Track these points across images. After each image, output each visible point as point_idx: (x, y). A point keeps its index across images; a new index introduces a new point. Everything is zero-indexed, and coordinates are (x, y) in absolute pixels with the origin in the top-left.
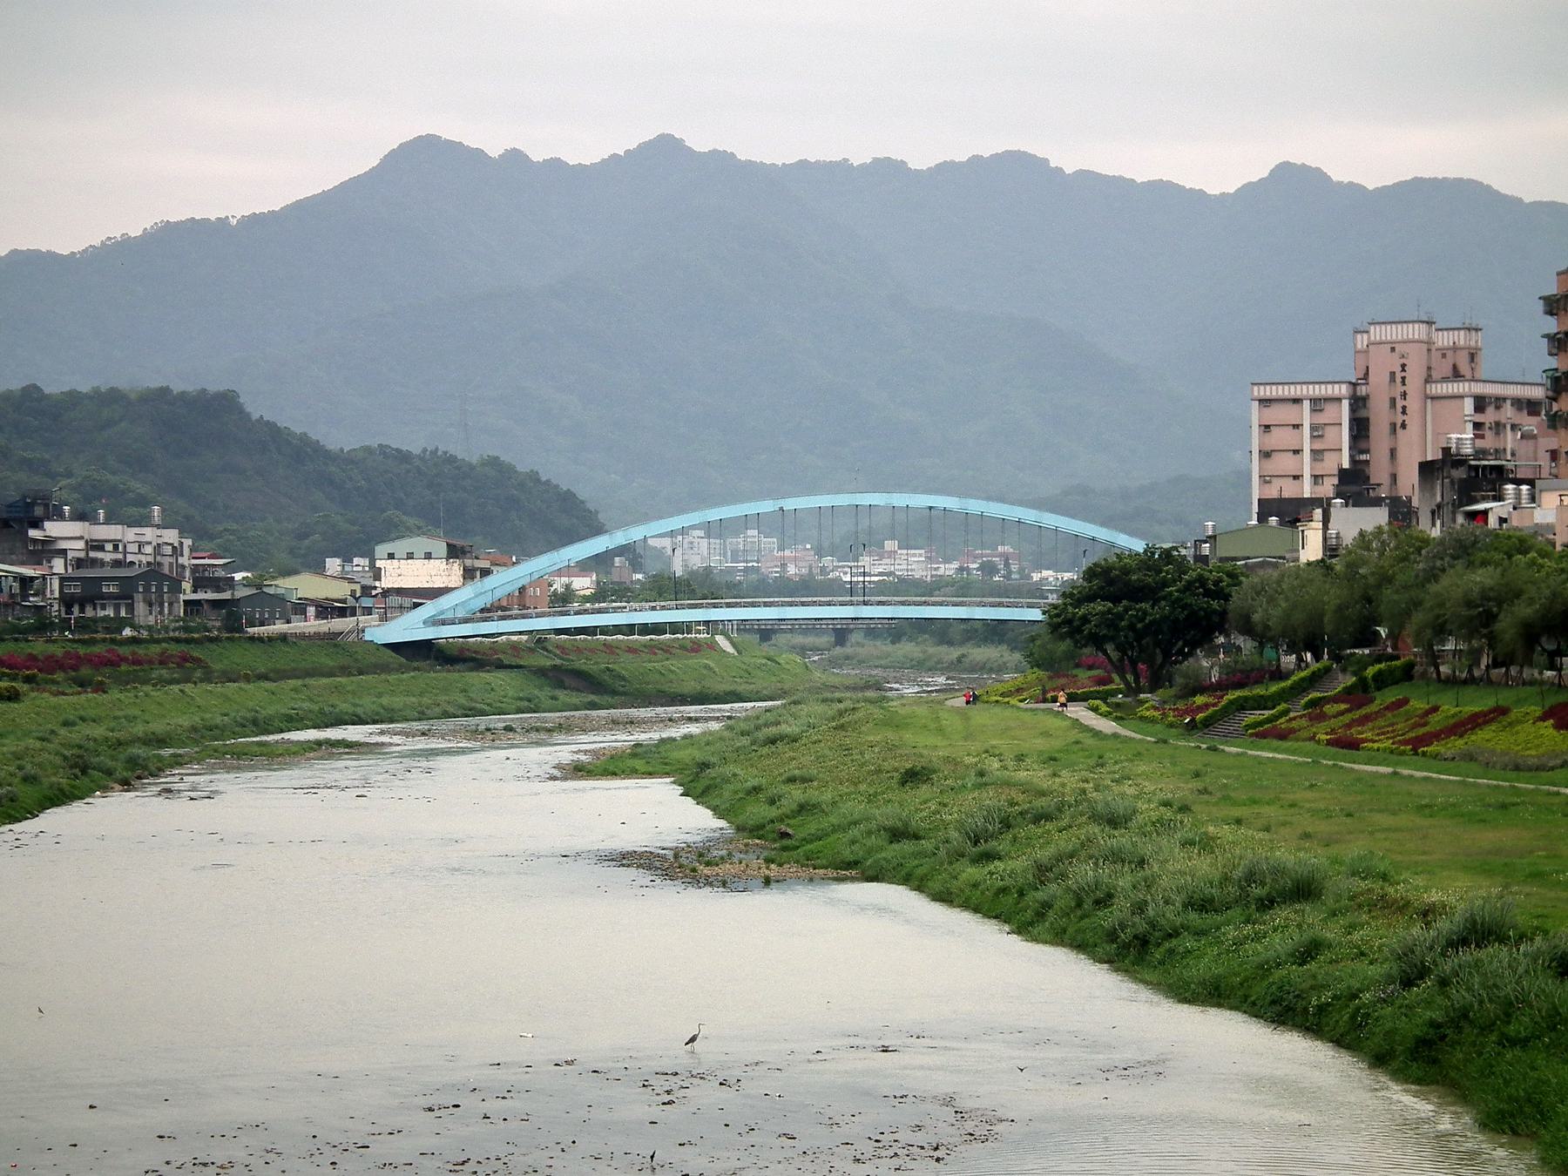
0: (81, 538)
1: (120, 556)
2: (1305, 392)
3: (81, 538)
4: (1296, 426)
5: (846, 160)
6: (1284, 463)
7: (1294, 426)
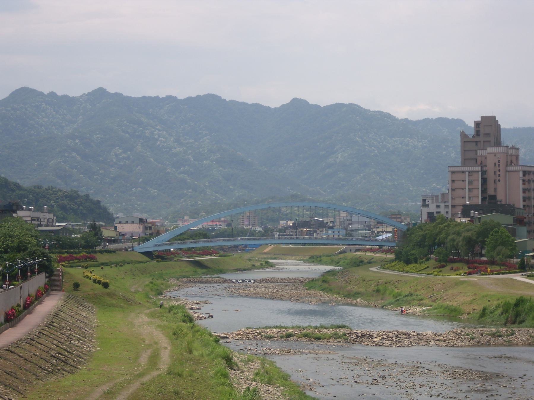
0: (30, 216)
1: (39, 223)
2: (466, 169)
3: (30, 216)
4: (463, 181)
5: (158, 96)
6: (459, 193)
7: (462, 180)
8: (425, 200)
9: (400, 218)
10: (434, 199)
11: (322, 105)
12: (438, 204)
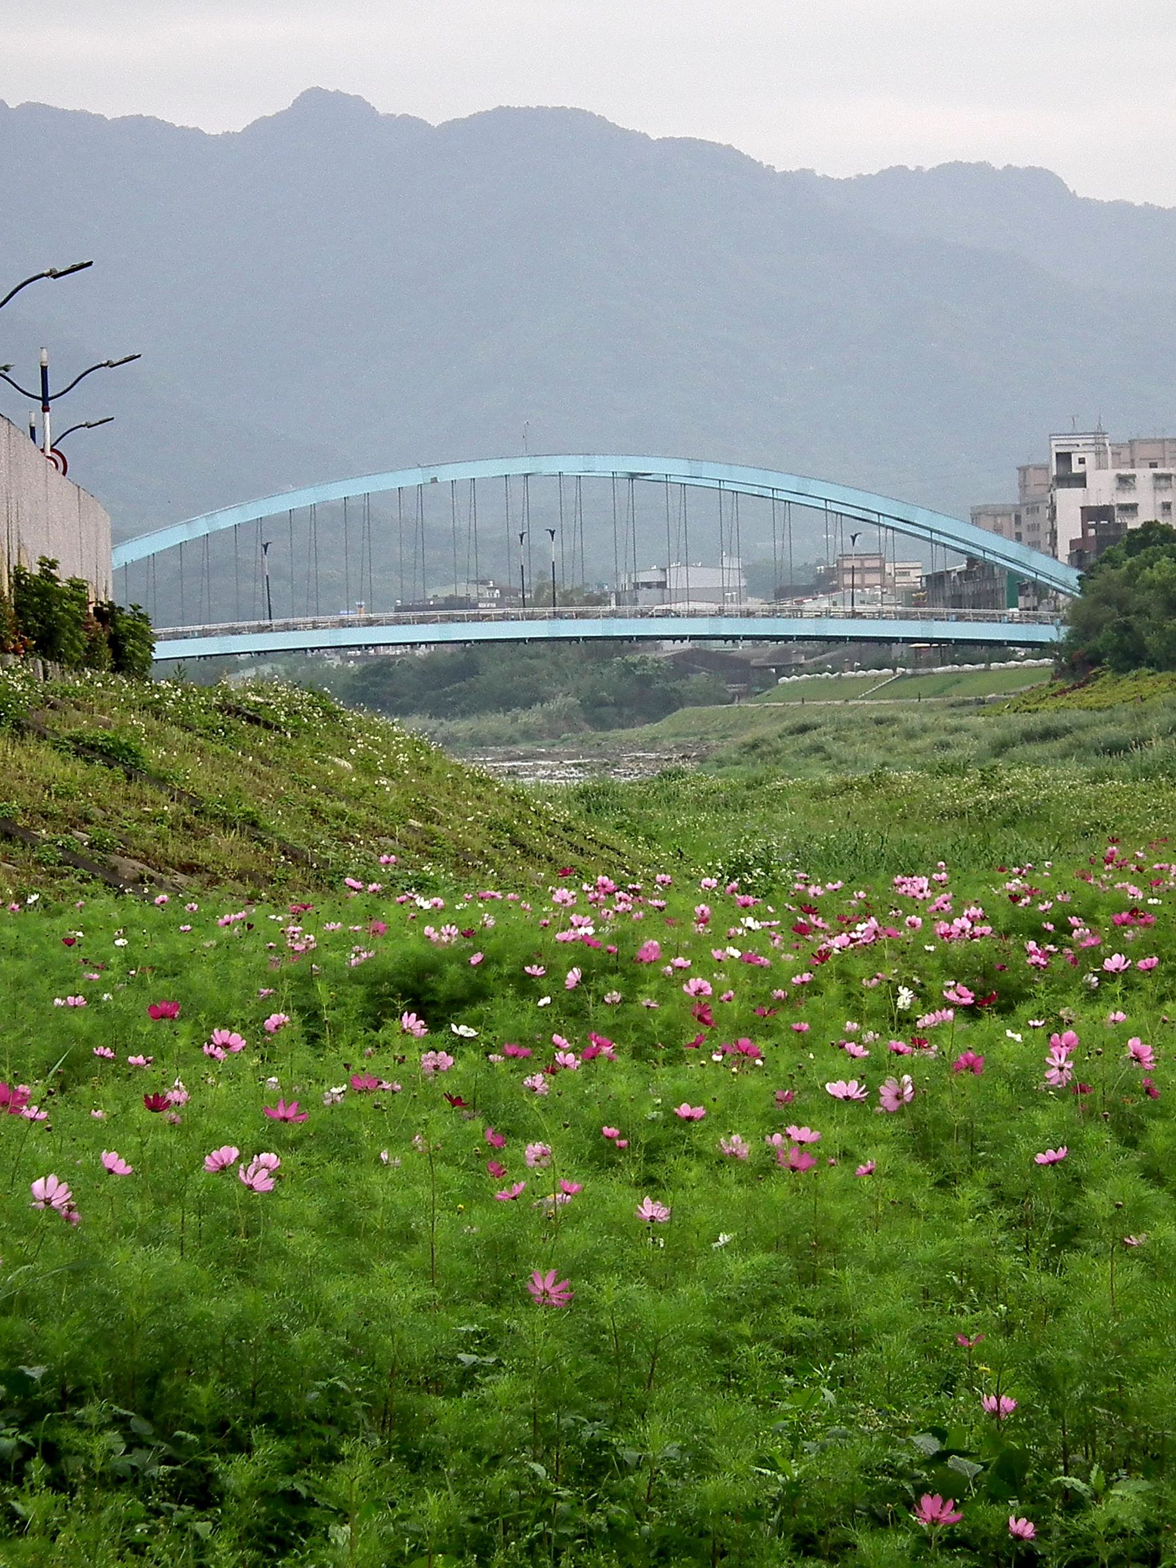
8: (1069, 454)
9: (881, 570)
10: (1106, 452)
11: (382, 108)
12: (1123, 472)
